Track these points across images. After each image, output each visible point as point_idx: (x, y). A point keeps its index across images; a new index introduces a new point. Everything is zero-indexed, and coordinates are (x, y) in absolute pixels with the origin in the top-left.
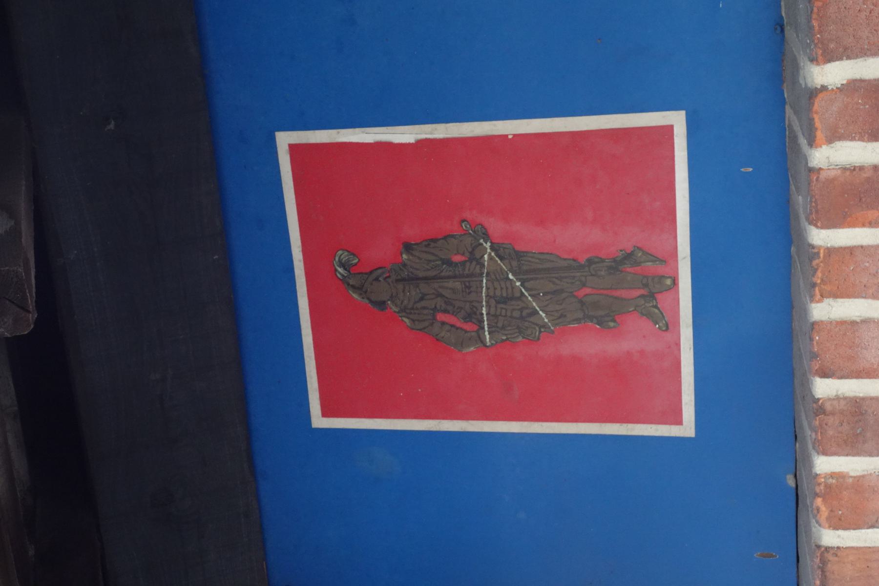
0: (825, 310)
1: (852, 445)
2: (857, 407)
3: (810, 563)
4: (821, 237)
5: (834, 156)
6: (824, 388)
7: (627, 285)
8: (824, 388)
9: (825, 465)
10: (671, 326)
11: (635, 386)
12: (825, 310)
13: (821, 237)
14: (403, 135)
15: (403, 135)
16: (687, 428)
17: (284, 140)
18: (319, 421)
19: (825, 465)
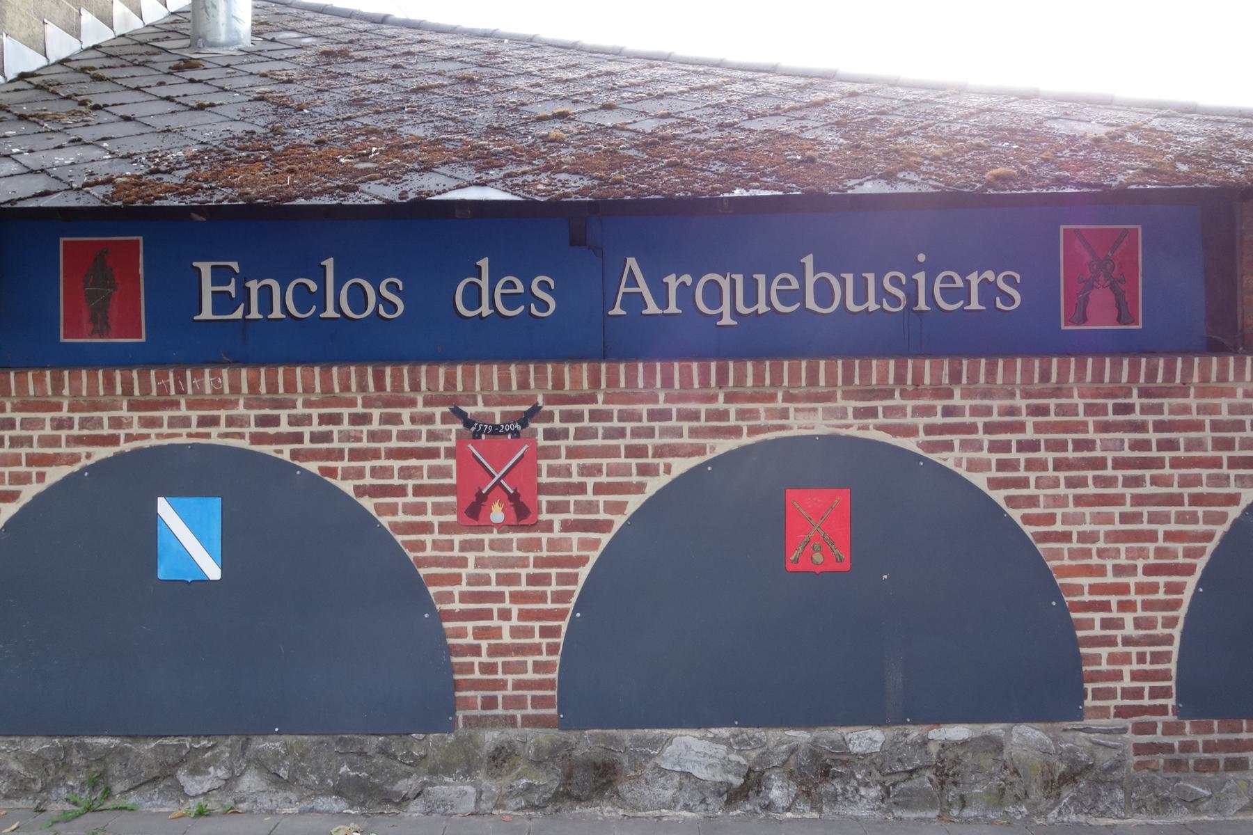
0: (84, 373)
1: (53, 379)
2: (62, 379)
3: (5, 370)
4: (100, 373)
5: (118, 375)
6: (66, 373)
7: (101, 325)
8: (478, 367)
9: (48, 373)
10: (91, 336)
11: (72, 330)
12: (84, 373)
13: (100, 373)
14: (141, 271)
15: (141, 271)
16: (62, 340)
17: (141, 239)
18: (62, 240)
19: (48, 373)
